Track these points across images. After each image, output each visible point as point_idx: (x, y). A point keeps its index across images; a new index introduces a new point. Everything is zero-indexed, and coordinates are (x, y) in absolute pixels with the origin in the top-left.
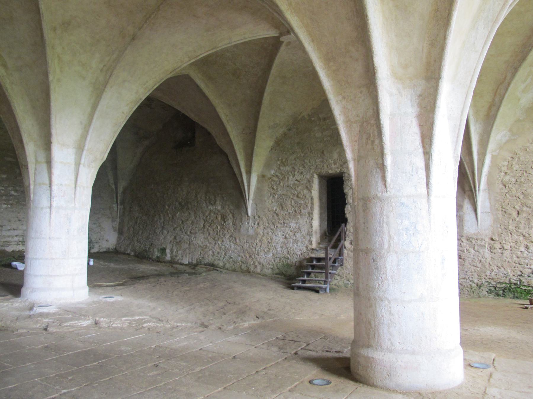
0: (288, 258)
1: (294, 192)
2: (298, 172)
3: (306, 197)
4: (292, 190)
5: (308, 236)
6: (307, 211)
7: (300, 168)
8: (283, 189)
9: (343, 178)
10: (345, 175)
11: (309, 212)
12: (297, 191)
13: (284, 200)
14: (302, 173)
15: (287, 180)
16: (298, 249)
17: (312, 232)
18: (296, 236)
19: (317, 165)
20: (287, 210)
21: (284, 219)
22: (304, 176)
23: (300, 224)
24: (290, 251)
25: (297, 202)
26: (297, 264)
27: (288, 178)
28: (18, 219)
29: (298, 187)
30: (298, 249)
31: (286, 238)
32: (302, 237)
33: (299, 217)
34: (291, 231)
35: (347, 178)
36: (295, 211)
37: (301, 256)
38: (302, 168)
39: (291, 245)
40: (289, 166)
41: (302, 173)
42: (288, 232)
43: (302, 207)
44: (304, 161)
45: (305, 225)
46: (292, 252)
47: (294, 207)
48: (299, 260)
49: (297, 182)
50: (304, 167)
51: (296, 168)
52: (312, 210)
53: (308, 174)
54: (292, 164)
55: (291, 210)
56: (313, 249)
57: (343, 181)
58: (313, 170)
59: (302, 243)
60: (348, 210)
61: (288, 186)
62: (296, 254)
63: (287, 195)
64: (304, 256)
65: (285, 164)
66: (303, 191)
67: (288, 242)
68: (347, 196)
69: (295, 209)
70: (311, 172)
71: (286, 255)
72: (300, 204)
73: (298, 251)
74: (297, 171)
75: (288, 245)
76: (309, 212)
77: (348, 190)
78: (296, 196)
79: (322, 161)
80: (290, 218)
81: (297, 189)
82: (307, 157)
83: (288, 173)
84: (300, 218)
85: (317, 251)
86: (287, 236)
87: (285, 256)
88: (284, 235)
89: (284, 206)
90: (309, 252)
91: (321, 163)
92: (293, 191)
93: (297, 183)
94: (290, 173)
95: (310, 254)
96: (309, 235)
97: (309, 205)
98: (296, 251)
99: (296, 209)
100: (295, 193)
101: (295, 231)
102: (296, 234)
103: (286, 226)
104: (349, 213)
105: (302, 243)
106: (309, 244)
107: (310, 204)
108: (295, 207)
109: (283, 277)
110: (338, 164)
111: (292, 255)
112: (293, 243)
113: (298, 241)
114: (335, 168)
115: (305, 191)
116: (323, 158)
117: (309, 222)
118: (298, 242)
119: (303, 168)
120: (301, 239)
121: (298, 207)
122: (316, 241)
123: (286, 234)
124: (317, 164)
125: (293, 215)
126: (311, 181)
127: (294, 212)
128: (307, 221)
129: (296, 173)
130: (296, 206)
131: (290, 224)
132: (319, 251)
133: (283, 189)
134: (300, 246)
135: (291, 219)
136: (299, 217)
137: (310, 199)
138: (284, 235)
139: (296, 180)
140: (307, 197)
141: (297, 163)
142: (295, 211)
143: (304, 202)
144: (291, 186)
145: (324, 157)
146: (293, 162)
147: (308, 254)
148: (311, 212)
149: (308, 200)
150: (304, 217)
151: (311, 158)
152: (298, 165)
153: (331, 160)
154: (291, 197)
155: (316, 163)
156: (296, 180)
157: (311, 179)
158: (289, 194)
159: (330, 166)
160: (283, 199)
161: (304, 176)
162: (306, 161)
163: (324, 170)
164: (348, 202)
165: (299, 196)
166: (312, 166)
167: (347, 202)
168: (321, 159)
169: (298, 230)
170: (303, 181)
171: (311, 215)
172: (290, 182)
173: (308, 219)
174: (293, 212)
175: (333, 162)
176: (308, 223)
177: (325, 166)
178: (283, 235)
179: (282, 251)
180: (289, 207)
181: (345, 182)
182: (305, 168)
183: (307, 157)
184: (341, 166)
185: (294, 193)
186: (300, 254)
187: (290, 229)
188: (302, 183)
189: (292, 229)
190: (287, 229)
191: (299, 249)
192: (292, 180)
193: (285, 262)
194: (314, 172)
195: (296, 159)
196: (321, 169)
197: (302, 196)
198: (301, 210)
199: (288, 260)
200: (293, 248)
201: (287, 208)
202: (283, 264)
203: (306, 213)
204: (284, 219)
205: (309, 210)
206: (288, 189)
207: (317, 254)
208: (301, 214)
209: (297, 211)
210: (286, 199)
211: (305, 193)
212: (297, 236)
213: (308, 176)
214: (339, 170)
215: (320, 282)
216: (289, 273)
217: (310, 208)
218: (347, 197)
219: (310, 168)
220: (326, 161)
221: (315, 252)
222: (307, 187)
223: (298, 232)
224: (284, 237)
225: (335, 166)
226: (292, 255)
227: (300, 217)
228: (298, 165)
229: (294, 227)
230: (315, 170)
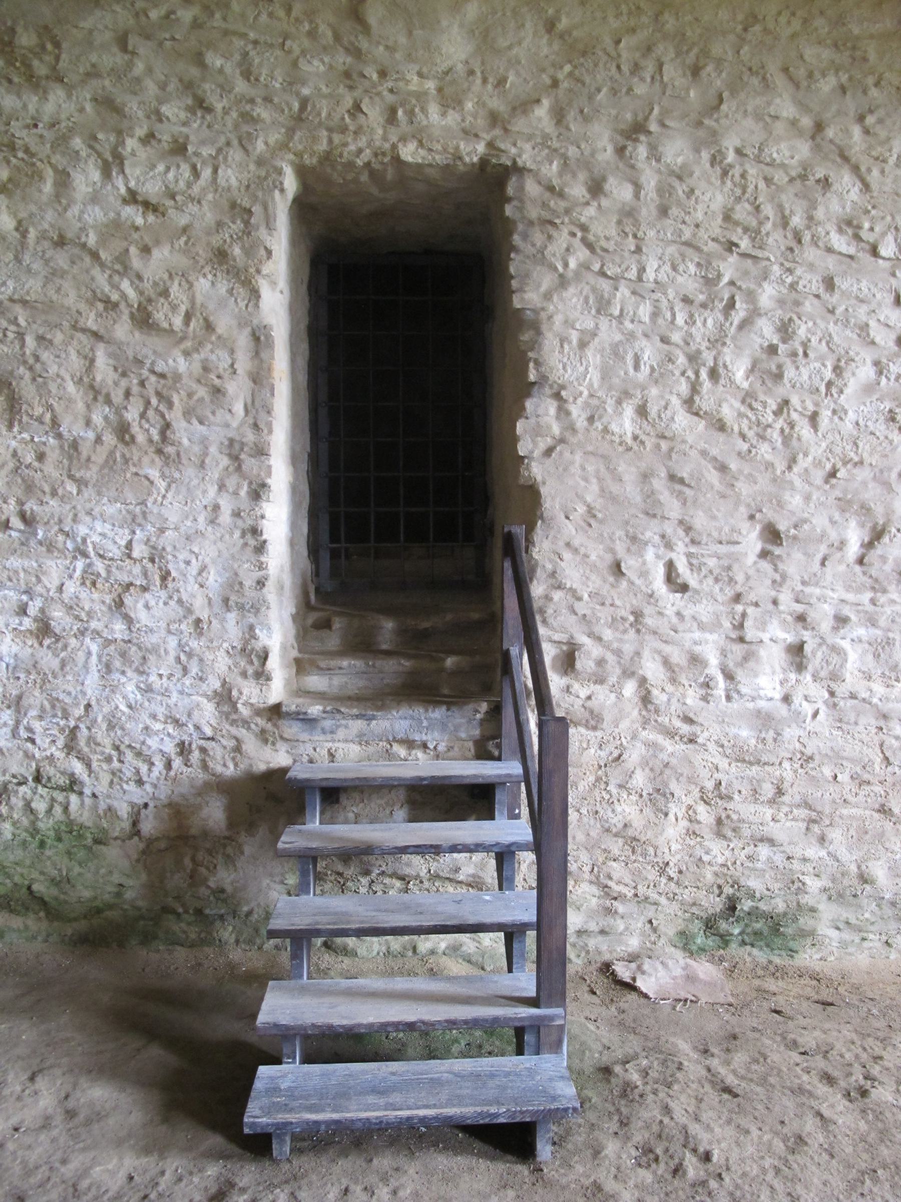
0: (73, 785)
1: (116, 287)
2: (149, 138)
3: (209, 327)
4: (96, 272)
5: (232, 617)
6: (216, 435)
7: (165, 109)
8: (18, 260)
9: (509, 210)
10: (521, 188)
11: (231, 441)
12: (140, 277)
13: (30, 341)
14: (179, 149)
15: (57, 196)
16: (154, 717)
17: (261, 583)
18: (129, 620)
19: (304, 103)
20: (55, 423)
21: (29, 488)
22: (196, 173)
23: (162, 531)
24: (84, 732)
25: (139, 362)
26: (148, 827)
27: (63, 180)
28: (799, 608)
29: (146, 250)
30: (154, 717)
31: (44, 629)
32: (186, 627)
33: (154, 474)
34: (90, 580)
35: (533, 213)
36: (123, 431)
37: (177, 763)
38: (183, 115)
39: (92, 680)
40: (69, 89)
41: (179, 149)
42: (60, 589)
43: (176, 399)
44: (199, 60)
45: (199, 533)
46: (100, 733)
47: (108, 401)
48: (163, 793)
49: (134, 215)
50: (201, 105)
51: (133, 106)
52: (256, 426)
53: (235, 154)
54: (94, 73)
55: (88, 423)
56: (276, 711)
57: (508, 226)
58: (275, 137)
59: (185, 671)
60: (538, 431)
61: (61, 242)
62: (139, 754)
63: (50, 306)
64: (205, 766)
65: (41, 69)
66: (191, 285)
67: (63, 665)
68: (539, 332)
69: (118, 412)
70: (260, 146)
71: (51, 759)
72: (162, 376)
73: (158, 726)
74: (140, 132)
75: (65, 686)
76: (231, 441)
77: (548, 296)
78: (126, 317)
79: (347, 75)
80: (81, 483)
81: (136, 262)
82: (226, 33)
83: (60, 143)
84: (162, 485)
85: (309, 722)
86: (57, 614)
87: (49, 770)
88: (33, 610)
89: (27, 389)
90: (242, 733)
91: (341, 90)
92: (101, 279)
93: (139, 221)
94: (77, 143)
95: (251, 745)
96: (241, 607)
97: (231, 387)
98: (135, 728)
99: (132, 415)
100: (124, 296)
101: (125, 578)
102: (135, 604)
103: (50, 547)
104: (549, 452)
105: (185, 671)
106: (244, 674)
107: (249, 384)
108: (118, 397)
109: (34, 923)
110: (469, 106)
111: (109, 759)
112: (108, 668)
113: (155, 650)
114: (447, 129)
115: (203, 285)
116: (357, 53)
117: (237, 514)
118: (152, 658)
119: (191, 110)
120: (172, 642)
121: (148, 403)
122: (284, 648)
123: (48, 600)
124: (306, 91)
125: (100, 456)
126: (257, 209)
127: (109, 439)
128: (216, 508)
129: (131, 143)
130: (128, 394)
131: (82, 530)
132: (328, 724)
133: (18, 260)
134: (166, 693)
135: (88, 493)
136: (154, 474)
137: (243, 341)
138: (33, 610)
139: (132, 197)
140: (224, 323)
141: (140, 67)
142: (123, 431)
143: (197, 367)
144: (92, 240)
145: (364, 44)
146: (112, 59)
147: (238, 749)
148: (250, 437)
149: (232, 352)
150: (190, 472)
151: (256, 43)
152: (151, 88)
153: (420, 74)
154: (91, 323)
155: (294, 80)
156: (132, 197)
157: (254, 198)
158: (71, 299)
159: (411, 114)
160: (21, 336)
161: (196, 173)
162: (215, 61)
163: (362, 142)
164: (543, 379)
165: (159, 316)
166: (268, 100)
167: (532, 377)
168: (342, 59)
169: (145, 574)
170: (193, 208)
171: (249, 463)
172: (75, 210)
173: (222, 487)
174: (98, 440)
175: (431, 85)
176: (225, 517)
177: (374, 114)
178: (23, 611)
179: (15, 734)
180: (70, 400)
181: (525, 237)
182: (209, 110)
183: (226, 33)
184: (494, 119)
185: (115, 297)
186: (170, 747)
187: (80, 564)
188: (183, 220)
189: (100, 566)
190: (54, 569)
191: (161, 711)
192: (95, 199)
193: (49, 811)
194: (284, 146)
195: (132, 41)
196: (344, 130)
197: (178, 322)
198: (167, 426)
199: (74, 798)
200: (106, 709)
201: (50, 407)
202: (34, 831)
203: (213, 450)
204: (29, 488)
205: (235, 424)
206: (61, 259)
207: (306, 750)
208: (170, 450)
209: (135, 429)
210: (41, 339)
211: (199, 299)
212: (142, 616)
213: (230, 176)
214: (481, 148)
215: (339, 940)
216: (87, 894)
217: (239, 408)
218: (534, 344)
219: (247, 117)
220: (383, 74)
221: (291, 729)
222: (221, 255)
223: (145, 589)
224: (27, 623)
225: (452, 118)
226: (109, 759)
227: (163, 476)
228: (151, 88)
229: (115, 552)
230: (291, 132)
